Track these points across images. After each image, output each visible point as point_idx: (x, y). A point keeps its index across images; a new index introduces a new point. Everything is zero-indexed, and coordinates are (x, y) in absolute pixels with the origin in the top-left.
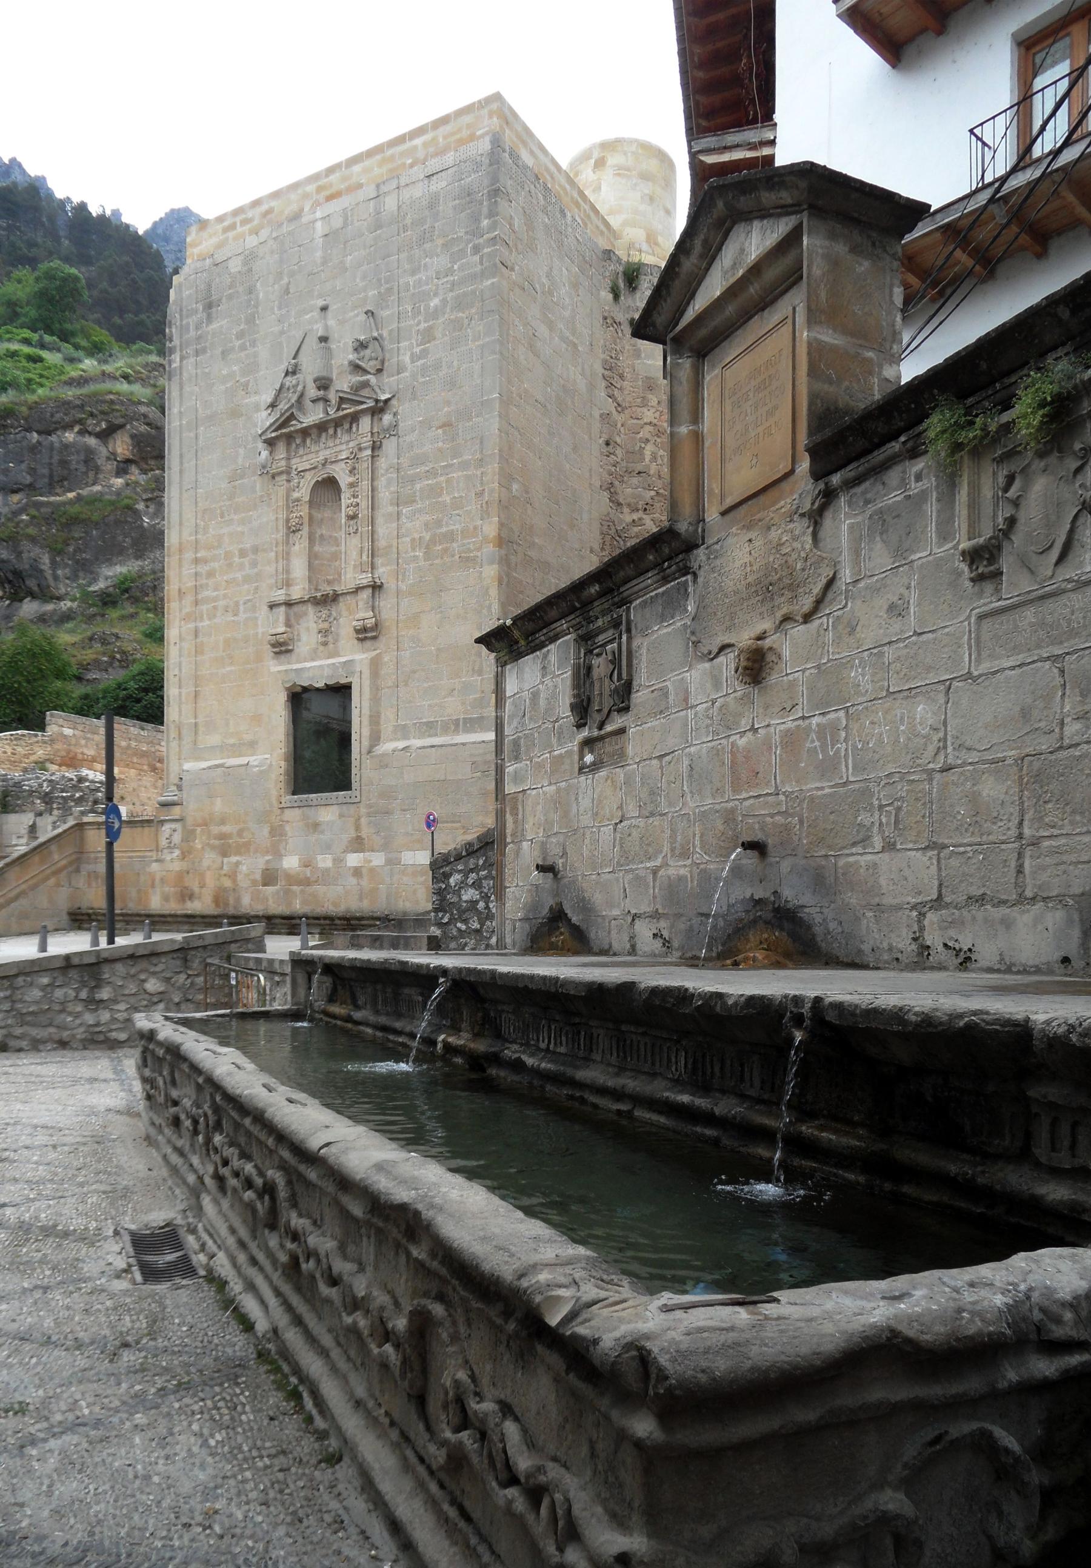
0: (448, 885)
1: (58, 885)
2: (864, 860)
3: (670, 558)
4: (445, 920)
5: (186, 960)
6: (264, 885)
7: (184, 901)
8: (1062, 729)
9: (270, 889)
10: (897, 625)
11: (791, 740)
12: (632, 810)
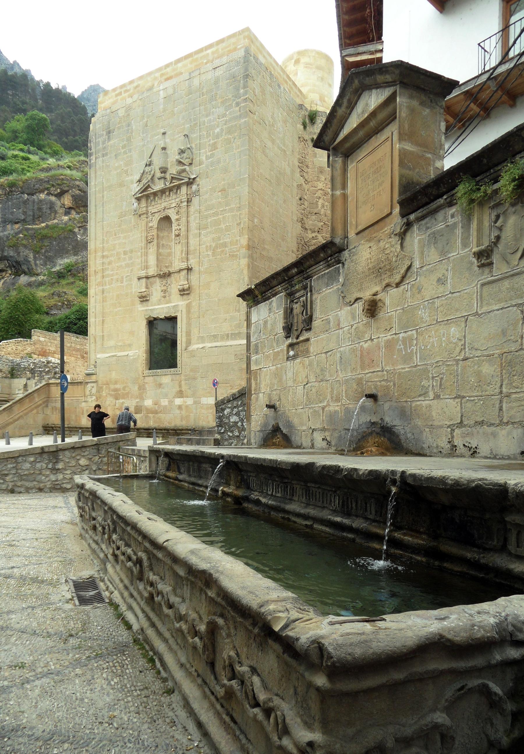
0: (224, 414)
2: (424, 403)
3: (331, 256)
4: (222, 431)
10: (441, 289)
11: (390, 345)
12: (312, 379)
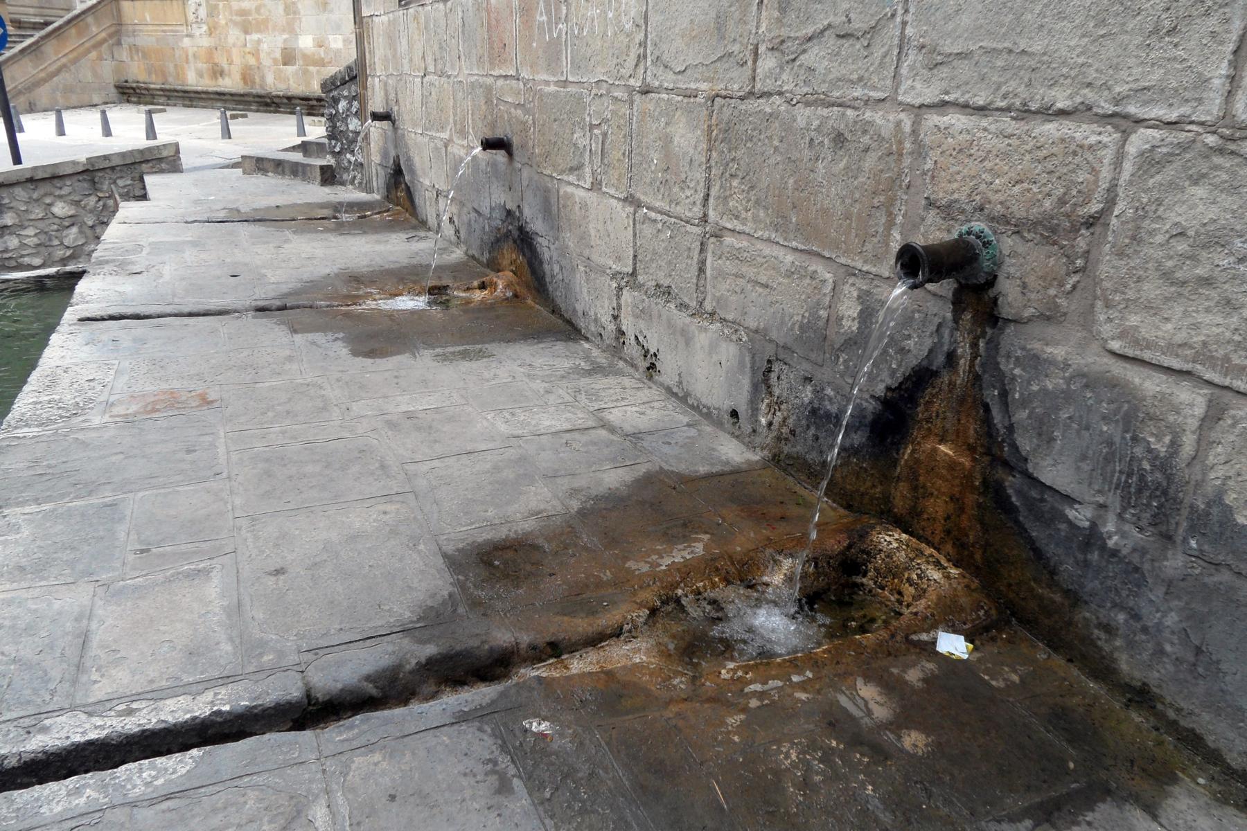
0: (337, 111)
1: (100, 58)
4: (337, 149)
5: (93, 182)
6: (285, 64)
7: (216, 79)
8: (755, 62)
9: (290, 69)
